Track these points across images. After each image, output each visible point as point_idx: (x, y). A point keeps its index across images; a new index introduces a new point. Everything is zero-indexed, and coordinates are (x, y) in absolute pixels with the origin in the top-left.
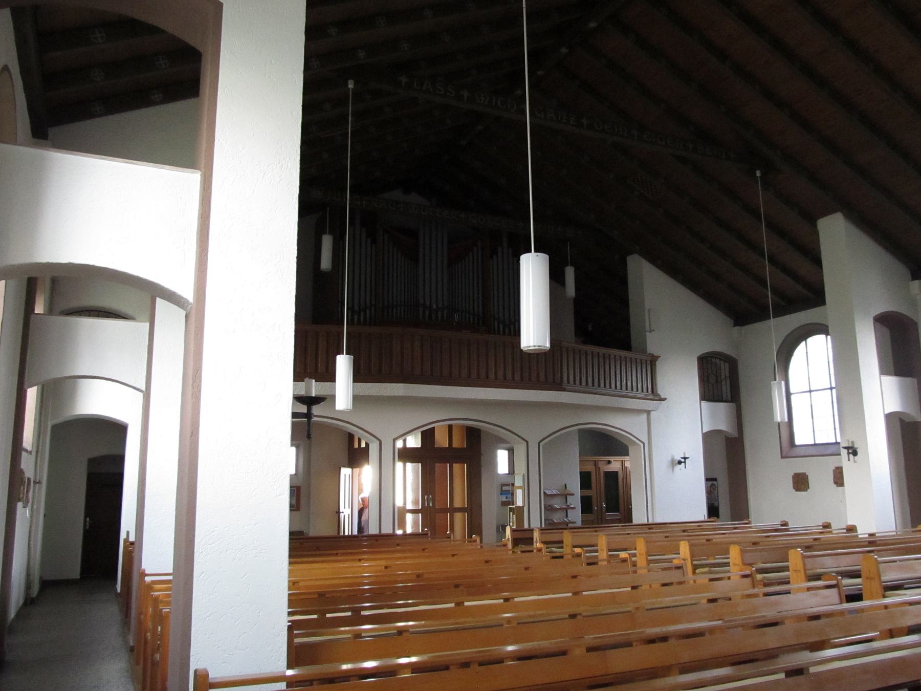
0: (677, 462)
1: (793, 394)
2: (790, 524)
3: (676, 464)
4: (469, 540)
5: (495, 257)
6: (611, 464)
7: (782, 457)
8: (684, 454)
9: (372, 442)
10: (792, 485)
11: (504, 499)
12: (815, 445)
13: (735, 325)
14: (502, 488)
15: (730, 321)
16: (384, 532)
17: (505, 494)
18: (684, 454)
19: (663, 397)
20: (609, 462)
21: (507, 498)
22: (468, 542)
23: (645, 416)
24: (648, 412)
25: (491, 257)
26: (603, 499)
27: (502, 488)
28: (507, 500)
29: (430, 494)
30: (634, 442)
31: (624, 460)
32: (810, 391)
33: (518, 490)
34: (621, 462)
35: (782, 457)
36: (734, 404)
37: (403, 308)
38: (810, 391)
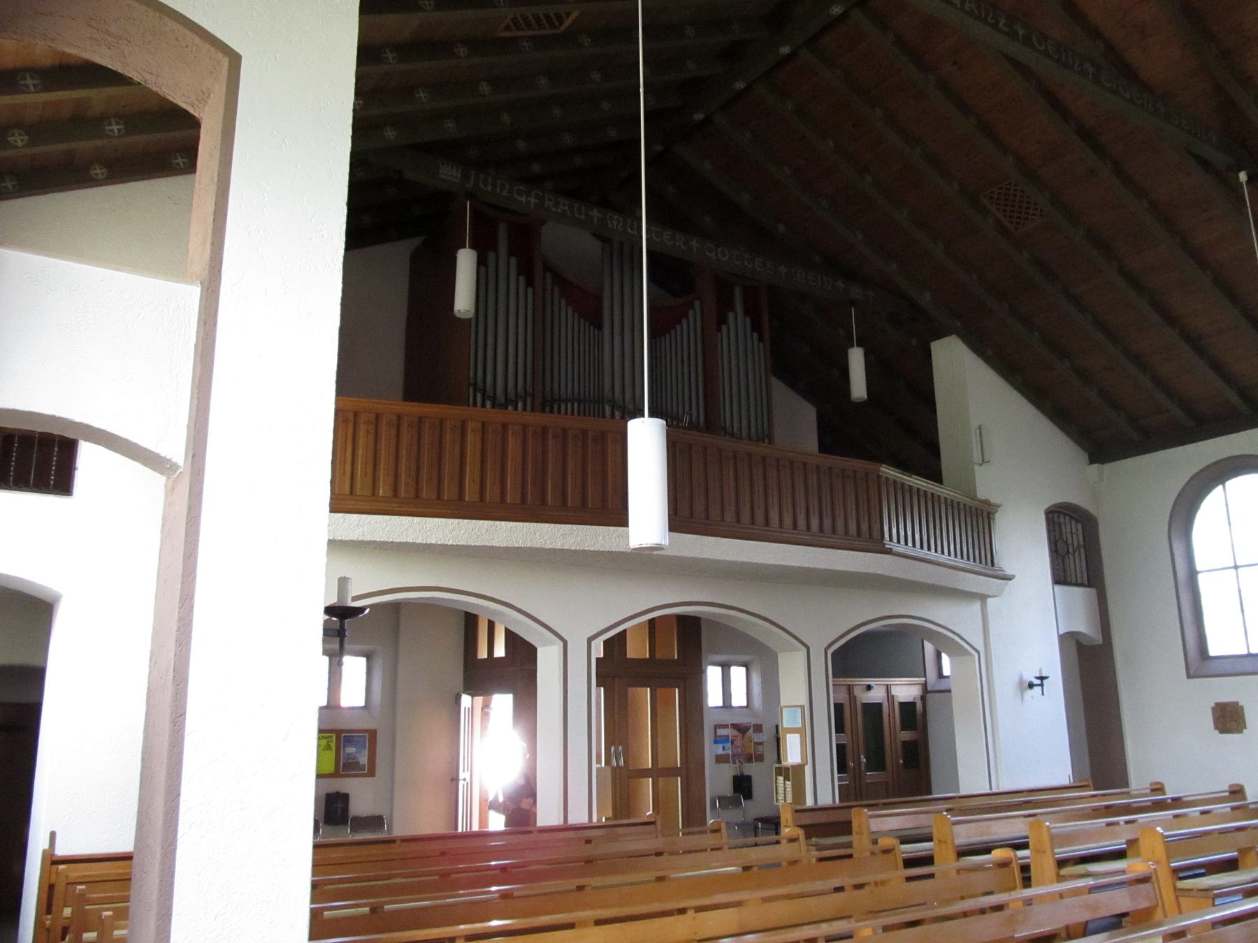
0: (1027, 684)
1: (1200, 572)
2: (1167, 789)
3: (1026, 689)
4: (686, 830)
5: (724, 328)
6: (872, 691)
7: (1189, 676)
8: (1041, 671)
9: (547, 643)
10: (1211, 724)
11: (720, 752)
12: (1249, 655)
13: (1092, 461)
14: (716, 732)
15: (1084, 456)
16: (573, 820)
17: (721, 742)
18: (1041, 671)
19: (1008, 572)
20: (869, 688)
21: (724, 748)
22: (683, 834)
23: (976, 606)
24: (983, 598)
25: (719, 330)
26: (862, 750)
27: (716, 732)
28: (724, 752)
29: (620, 744)
30: (966, 650)
31: (853, 685)
32: (1236, 567)
33: (789, 736)
34: (847, 686)
35: (1189, 676)
36: (1093, 591)
37: (587, 406)
38: (1236, 567)
